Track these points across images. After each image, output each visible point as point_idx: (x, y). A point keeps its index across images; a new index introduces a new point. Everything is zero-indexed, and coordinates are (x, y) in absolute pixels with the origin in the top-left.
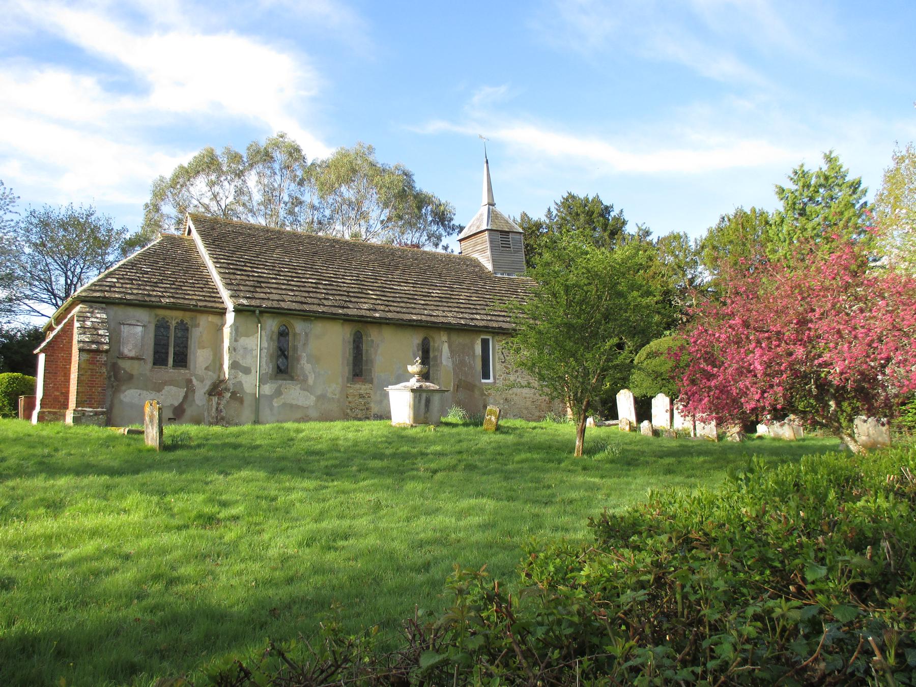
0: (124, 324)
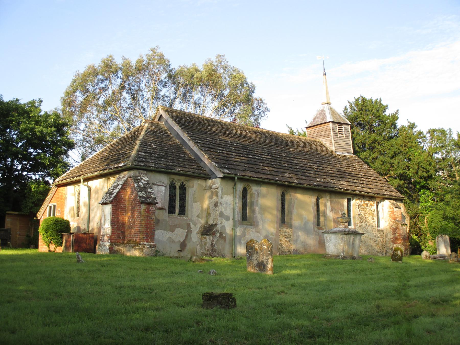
0: (155, 185)
